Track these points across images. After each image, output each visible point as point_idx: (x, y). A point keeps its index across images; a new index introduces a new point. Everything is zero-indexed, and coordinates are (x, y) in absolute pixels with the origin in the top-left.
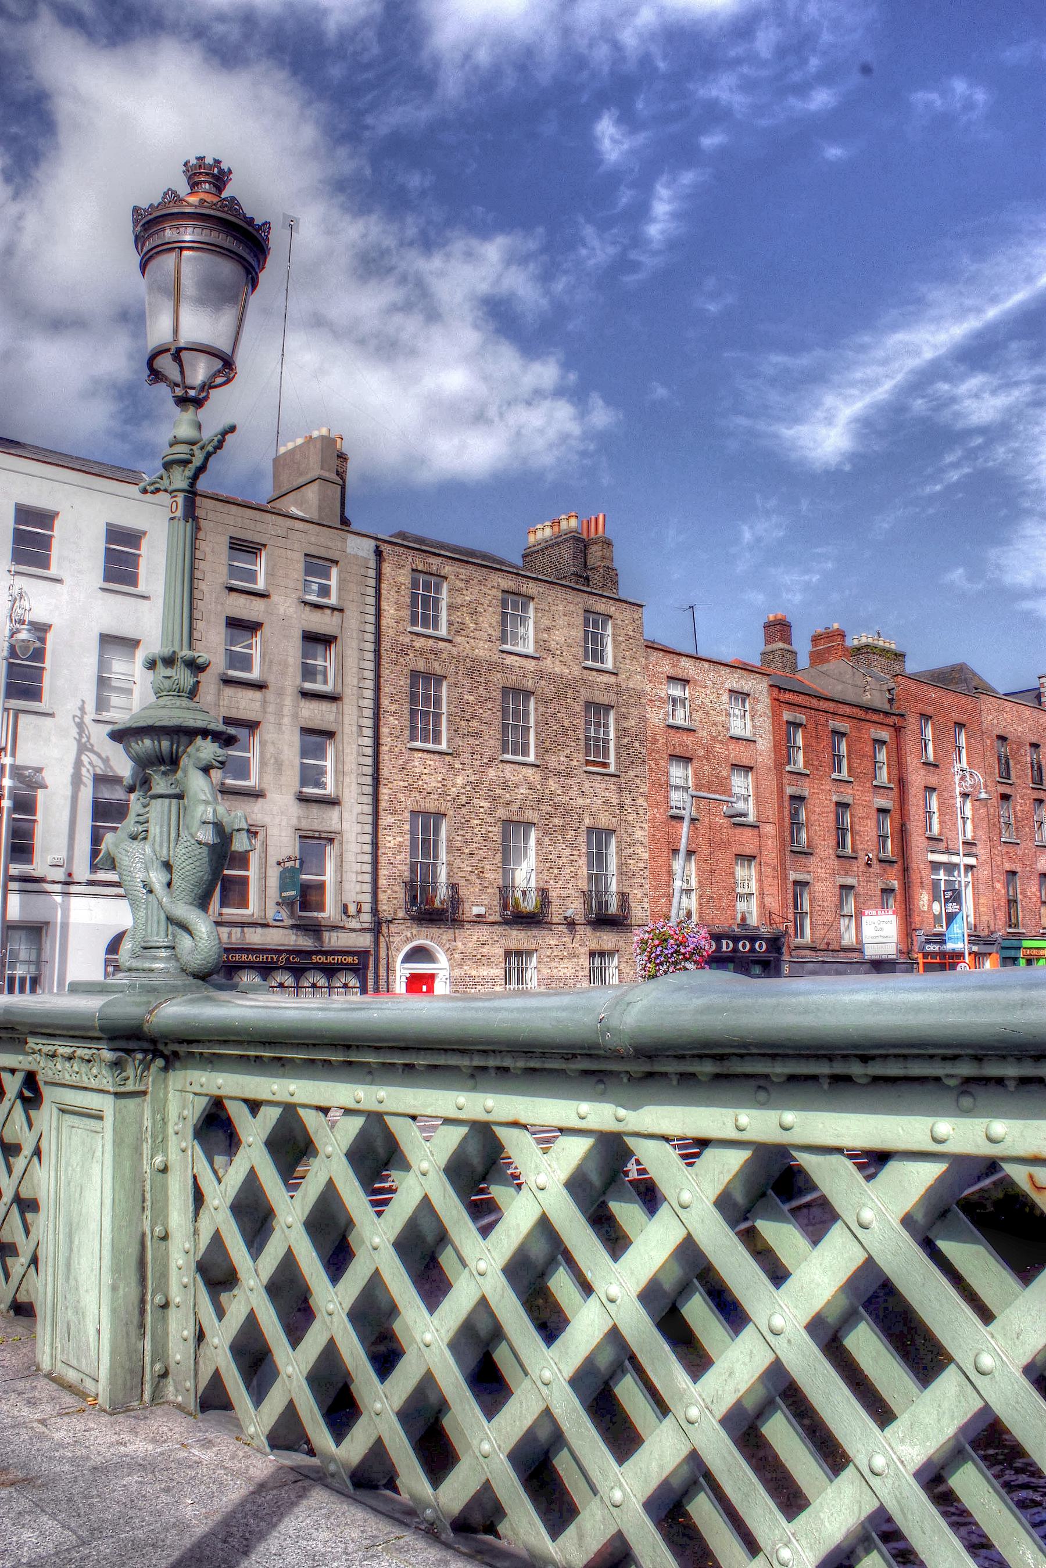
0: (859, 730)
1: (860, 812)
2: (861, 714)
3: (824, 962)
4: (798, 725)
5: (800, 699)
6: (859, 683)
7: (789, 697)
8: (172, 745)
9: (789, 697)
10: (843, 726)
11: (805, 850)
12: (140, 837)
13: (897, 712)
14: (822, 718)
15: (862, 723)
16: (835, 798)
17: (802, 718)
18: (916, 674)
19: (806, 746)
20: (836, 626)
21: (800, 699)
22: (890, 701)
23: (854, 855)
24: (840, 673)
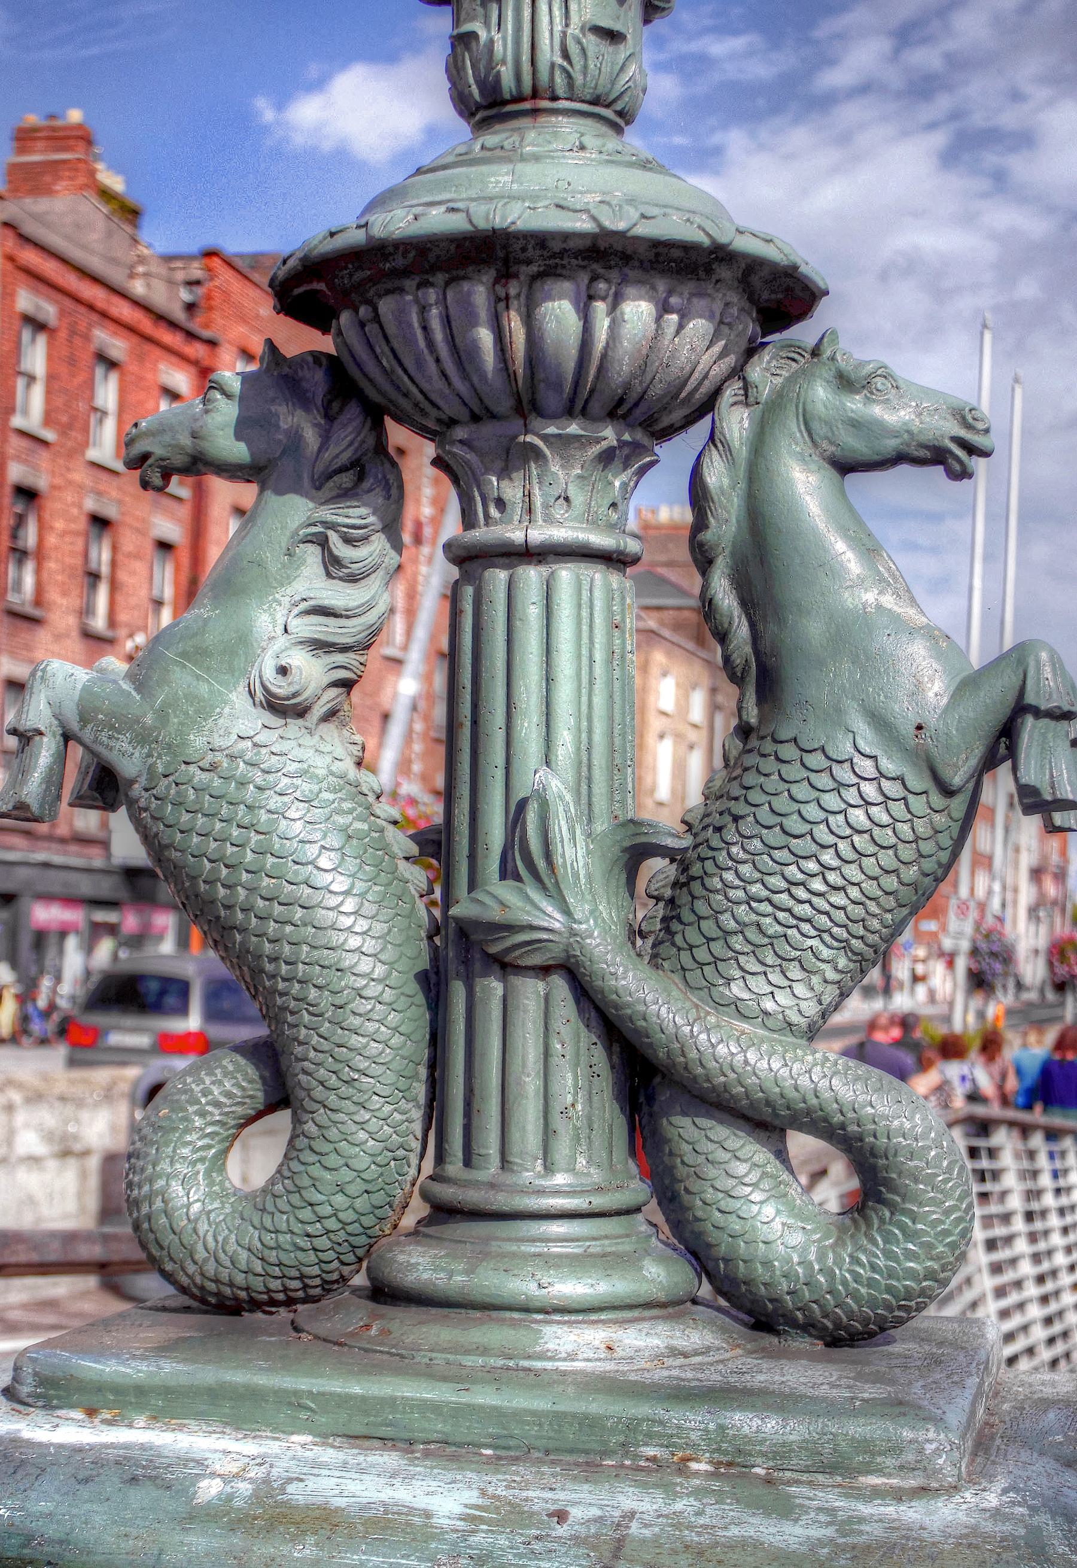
0: (141, 358)
1: (129, 541)
2: (146, 324)
3: (46, 865)
4: (38, 326)
5: (49, 268)
6: (119, 254)
7: (30, 257)
8: (40, 138)
9: (30, 257)
10: (117, 346)
11: (29, 610)
12: (318, 711)
13: (206, 334)
14: (84, 316)
15: (147, 347)
16: (90, 504)
17: (49, 310)
18: (578, 311)
19: (51, 377)
20: (75, 116)
21: (49, 268)
22: (190, 307)
23: (109, 634)
24: (78, 226)
